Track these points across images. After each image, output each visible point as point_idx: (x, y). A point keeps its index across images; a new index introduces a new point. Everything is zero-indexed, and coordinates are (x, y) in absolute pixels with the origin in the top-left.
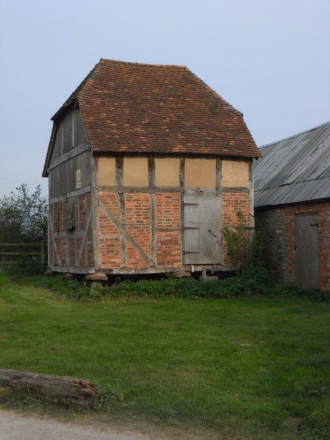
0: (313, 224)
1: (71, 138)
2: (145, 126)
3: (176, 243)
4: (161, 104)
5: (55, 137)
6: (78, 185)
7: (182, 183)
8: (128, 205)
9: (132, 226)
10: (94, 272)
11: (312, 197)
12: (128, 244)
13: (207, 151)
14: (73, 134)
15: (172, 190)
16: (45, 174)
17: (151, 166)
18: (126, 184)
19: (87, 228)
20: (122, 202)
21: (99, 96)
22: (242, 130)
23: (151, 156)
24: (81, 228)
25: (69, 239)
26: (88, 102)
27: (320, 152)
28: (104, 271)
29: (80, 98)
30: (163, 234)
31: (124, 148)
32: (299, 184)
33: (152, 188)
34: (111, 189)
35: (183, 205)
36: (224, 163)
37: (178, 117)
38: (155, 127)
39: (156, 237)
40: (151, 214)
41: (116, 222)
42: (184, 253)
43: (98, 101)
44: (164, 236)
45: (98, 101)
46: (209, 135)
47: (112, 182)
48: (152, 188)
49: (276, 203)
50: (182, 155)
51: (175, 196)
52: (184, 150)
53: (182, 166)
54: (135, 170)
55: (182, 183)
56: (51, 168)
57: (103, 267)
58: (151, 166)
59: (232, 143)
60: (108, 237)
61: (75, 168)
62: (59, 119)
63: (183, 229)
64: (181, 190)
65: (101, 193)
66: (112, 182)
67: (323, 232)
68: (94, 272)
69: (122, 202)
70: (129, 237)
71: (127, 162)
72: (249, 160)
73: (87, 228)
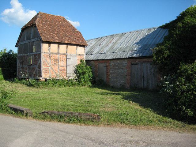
0: (105, 66)
1: (31, 36)
2: (56, 34)
3: (65, 70)
4: (59, 28)
5: (21, 35)
6: (34, 51)
7: (67, 52)
8: (51, 58)
9: (53, 65)
10: (41, 79)
11: (106, 57)
12: (51, 70)
13: (74, 43)
14: (32, 34)
15: (64, 54)
16: (16, 46)
17: (59, 47)
18: (51, 51)
19: (38, 65)
20: (50, 57)
21: (41, 23)
22: (82, 37)
23: (59, 43)
24: (35, 65)
25: (28, 68)
26: (39, 25)
27: (102, 45)
28: (44, 78)
29: (36, 23)
30: (61, 67)
31: (52, 41)
32: (98, 55)
33: (58, 53)
34: (47, 53)
35: (67, 59)
36: (60, 46)
37: (65, 32)
38: (59, 35)
39: (59, 68)
40: (58, 61)
41: (48, 63)
42: (67, 73)
43: (41, 25)
44: (61, 68)
45: (41, 25)
46: (74, 38)
47: (48, 51)
48: (58, 53)
49: (91, 59)
50: (67, 44)
51: (65, 56)
52: (68, 42)
53: (67, 47)
54: (54, 47)
55: (67, 52)
56: (19, 44)
57: (44, 77)
58: (59, 47)
59: (80, 41)
60: (46, 68)
61: (32, 45)
62: (23, 30)
63: (67, 66)
64: (66, 54)
65: (44, 54)
66: (48, 51)
67: (108, 68)
68: (41, 79)
69: (50, 57)
70: (51, 68)
71: (52, 45)
72: (84, 46)
73: (38, 65)
